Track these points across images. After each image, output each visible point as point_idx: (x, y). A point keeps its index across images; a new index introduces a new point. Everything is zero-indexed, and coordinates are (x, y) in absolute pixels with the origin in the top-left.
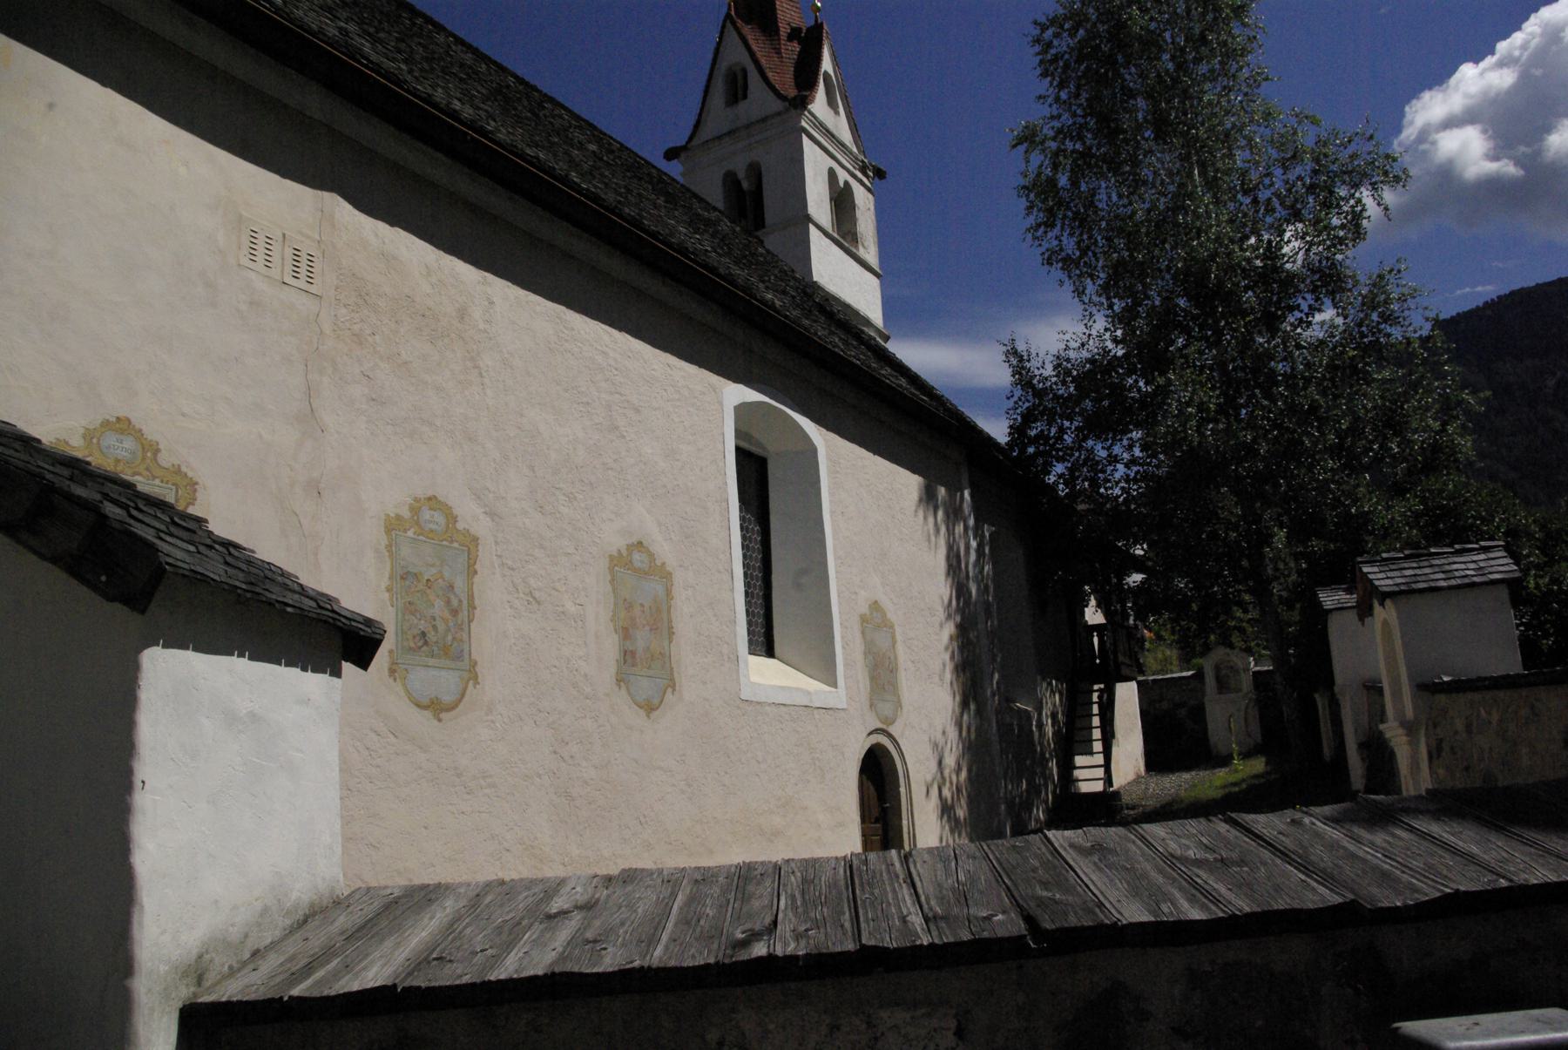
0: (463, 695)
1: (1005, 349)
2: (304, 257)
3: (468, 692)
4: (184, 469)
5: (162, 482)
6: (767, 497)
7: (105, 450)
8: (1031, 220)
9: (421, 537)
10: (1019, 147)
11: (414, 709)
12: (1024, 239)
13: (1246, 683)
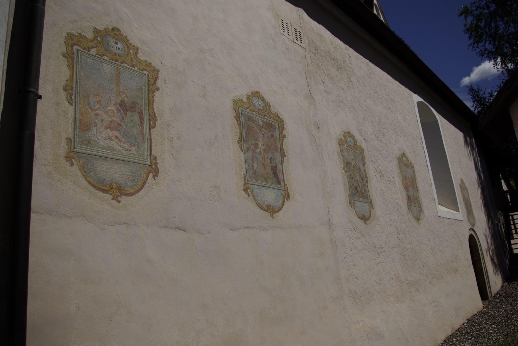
1: (468, 89)
2: (298, 33)
4: (279, 115)
7: (254, 105)
8: (471, 41)
9: (348, 148)
10: (462, 16)
11: (359, 219)
12: (469, 48)
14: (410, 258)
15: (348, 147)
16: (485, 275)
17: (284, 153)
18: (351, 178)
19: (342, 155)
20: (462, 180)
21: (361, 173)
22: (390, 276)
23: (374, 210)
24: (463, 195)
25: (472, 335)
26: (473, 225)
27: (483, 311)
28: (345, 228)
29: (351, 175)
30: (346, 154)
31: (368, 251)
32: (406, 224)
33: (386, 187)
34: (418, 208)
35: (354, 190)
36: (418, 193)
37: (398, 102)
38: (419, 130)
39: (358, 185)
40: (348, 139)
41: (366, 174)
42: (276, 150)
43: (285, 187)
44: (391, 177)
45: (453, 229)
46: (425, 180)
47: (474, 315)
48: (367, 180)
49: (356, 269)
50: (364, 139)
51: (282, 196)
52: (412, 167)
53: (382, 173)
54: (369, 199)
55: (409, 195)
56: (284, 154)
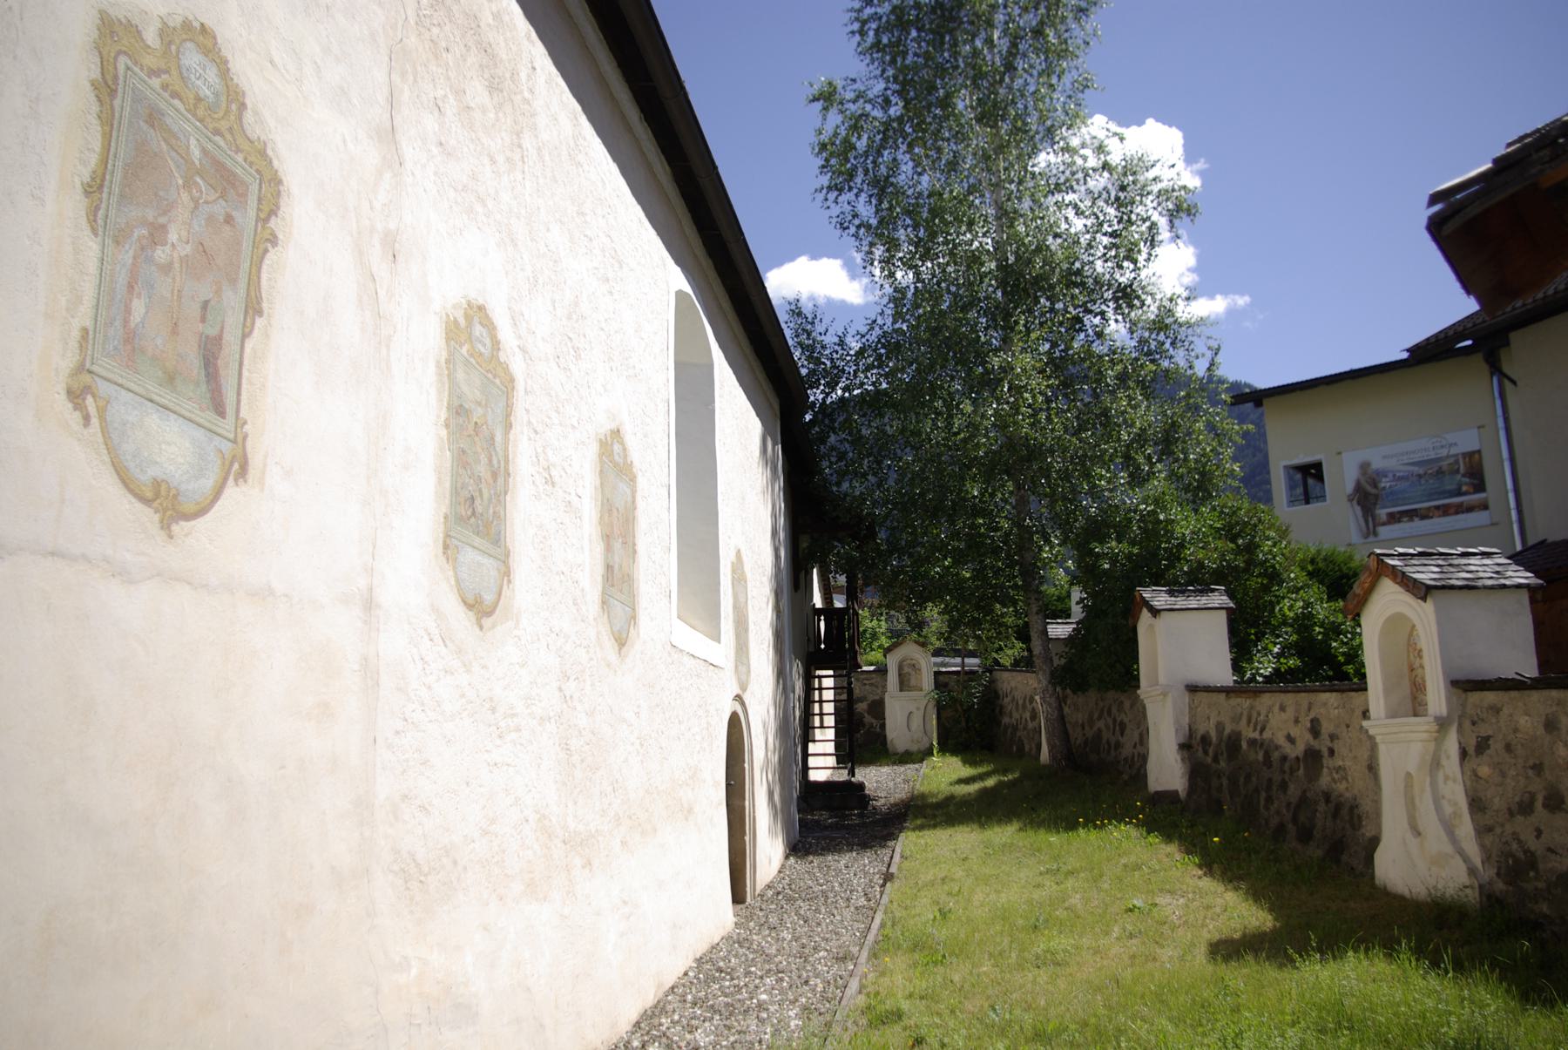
0: (500, 594)
3: (503, 593)
5: (245, 160)
6: (1365, 369)
9: (472, 360)
13: (927, 682)
14: (582, 761)
15: (472, 355)
17: (259, 300)
18: (462, 460)
19: (449, 376)
20: (739, 552)
21: (493, 453)
23: (511, 586)
25: (712, 1006)
26: (744, 687)
27: (735, 938)
30: (460, 375)
31: (472, 720)
33: (555, 520)
34: (627, 609)
39: (480, 491)
40: (478, 330)
42: (233, 281)
43: (239, 430)
44: (573, 493)
48: (506, 483)
50: (523, 349)
51: (219, 462)
52: (633, 479)
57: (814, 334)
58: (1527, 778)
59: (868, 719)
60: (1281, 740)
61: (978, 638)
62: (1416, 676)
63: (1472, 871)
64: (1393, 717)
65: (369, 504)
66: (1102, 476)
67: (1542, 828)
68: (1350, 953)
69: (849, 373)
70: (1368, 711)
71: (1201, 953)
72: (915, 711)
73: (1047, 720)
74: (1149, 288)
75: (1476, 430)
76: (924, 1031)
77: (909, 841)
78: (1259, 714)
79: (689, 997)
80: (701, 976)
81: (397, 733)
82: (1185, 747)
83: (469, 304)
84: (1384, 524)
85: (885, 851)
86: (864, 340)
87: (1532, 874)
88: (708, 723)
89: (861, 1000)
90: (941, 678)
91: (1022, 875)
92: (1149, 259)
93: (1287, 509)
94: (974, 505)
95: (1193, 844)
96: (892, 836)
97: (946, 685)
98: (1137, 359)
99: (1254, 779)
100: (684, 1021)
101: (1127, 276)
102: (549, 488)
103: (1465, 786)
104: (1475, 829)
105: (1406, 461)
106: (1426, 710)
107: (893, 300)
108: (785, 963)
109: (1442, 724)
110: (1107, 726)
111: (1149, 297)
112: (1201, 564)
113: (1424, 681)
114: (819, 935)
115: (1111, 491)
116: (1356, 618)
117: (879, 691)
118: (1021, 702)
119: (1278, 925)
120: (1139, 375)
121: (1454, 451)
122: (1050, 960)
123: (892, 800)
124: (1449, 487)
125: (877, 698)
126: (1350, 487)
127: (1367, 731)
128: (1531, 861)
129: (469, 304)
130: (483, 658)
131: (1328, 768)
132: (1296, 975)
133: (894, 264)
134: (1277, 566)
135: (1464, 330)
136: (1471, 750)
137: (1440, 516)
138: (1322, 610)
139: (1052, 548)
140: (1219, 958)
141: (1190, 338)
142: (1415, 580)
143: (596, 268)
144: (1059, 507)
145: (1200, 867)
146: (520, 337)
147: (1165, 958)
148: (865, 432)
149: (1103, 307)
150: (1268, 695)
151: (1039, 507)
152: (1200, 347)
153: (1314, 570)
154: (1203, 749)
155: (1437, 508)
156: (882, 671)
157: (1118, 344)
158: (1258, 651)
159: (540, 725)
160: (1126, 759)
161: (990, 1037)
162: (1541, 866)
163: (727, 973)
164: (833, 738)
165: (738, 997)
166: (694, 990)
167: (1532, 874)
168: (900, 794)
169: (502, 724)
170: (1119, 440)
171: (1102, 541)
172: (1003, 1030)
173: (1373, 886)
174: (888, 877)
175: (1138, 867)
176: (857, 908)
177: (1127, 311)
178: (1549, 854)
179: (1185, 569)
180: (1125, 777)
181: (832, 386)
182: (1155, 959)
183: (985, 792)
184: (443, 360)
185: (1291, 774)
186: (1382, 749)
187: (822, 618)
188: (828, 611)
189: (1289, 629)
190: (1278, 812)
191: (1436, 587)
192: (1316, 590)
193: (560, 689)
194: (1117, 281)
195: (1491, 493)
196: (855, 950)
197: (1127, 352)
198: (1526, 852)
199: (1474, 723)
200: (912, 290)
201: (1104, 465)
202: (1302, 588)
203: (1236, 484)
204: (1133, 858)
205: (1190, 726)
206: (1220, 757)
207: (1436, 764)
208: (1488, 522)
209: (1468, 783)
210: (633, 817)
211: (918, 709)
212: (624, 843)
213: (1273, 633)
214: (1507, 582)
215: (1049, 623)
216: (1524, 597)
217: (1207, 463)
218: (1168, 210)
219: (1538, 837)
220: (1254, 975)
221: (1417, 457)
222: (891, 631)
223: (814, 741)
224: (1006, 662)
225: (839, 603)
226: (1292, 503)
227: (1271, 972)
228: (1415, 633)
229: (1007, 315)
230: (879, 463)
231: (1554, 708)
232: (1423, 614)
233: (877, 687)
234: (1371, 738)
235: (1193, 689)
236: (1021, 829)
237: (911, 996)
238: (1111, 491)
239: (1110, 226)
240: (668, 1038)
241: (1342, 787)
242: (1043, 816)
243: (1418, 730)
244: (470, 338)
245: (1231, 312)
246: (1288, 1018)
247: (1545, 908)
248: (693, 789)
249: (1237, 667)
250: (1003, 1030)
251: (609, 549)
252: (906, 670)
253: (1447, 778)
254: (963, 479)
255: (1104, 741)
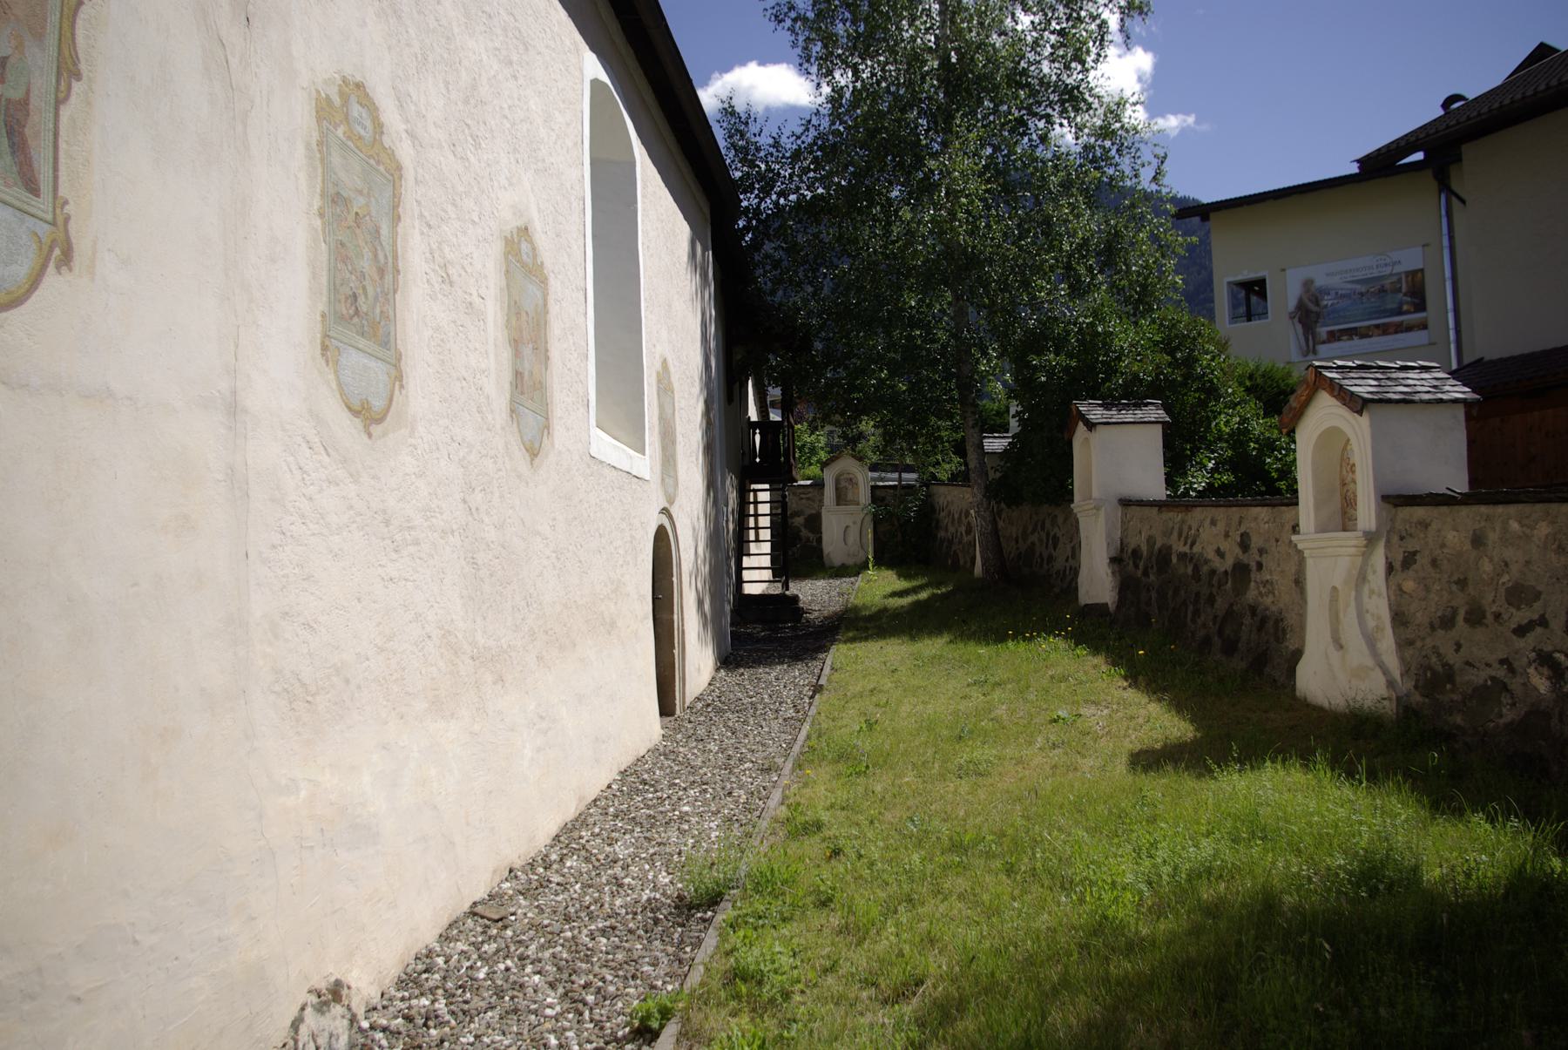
0: (391, 400)
3: (395, 399)
9: (349, 143)
13: (864, 496)
14: (491, 575)
15: (349, 138)
16: (676, 645)
17: (75, 61)
18: (341, 254)
19: (322, 160)
20: (665, 362)
21: (379, 248)
22: (423, 628)
23: (404, 392)
24: (661, 407)
25: (634, 818)
26: (671, 501)
27: (662, 749)
28: (290, 437)
29: (342, 244)
30: (336, 160)
31: (361, 533)
32: (495, 463)
33: (454, 322)
34: (539, 417)
35: (346, 302)
36: (546, 369)
37: (539, 53)
38: (582, 170)
39: (364, 288)
40: (356, 110)
41: (397, 256)
42: (39, 37)
43: (58, 211)
44: (475, 294)
45: (621, 501)
46: (572, 334)
47: (640, 760)
48: (395, 281)
49: (312, 594)
50: (412, 135)
51: (34, 246)
52: (544, 281)
53: (450, 272)
54: (393, 351)
55: (521, 370)
56: (75, 64)
57: (748, 135)
58: (1451, 593)
59: (805, 533)
60: (1210, 554)
61: (915, 452)
62: (1348, 491)
63: (1391, 684)
64: (1324, 531)
65: (229, 299)
66: (1042, 287)
67: (1462, 642)
68: (1268, 763)
69: (785, 177)
70: (1298, 525)
71: (1121, 767)
72: (851, 524)
73: (981, 534)
74: (1097, 90)
75: (1421, 248)
76: (842, 842)
77: (839, 654)
78: (1190, 528)
79: (612, 809)
80: (625, 788)
81: (274, 547)
82: (1114, 560)
83: (344, 80)
84: (1324, 342)
85: (815, 663)
86: (799, 142)
87: (1448, 686)
88: (632, 537)
89: (783, 812)
90: (878, 492)
91: (950, 687)
92: (1098, 60)
93: (1228, 326)
94: (912, 317)
95: (1120, 657)
96: (824, 649)
97: (883, 499)
98: (1081, 166)
99: (1182, 592)
100: (605, 834)
101: (1074, 77)
102: (446, 287)
103: (1389, 600)
104: (1396, 643)
105: (1349, 279)
106: (1356, 524)
107: (831, 100)
108: (709, 775)
109: (1371, 539)
110: (1040, 540)
111: (1096, 101)
112: (1136, 376)
113: (1355, 496)
114: (745, 746)
115: (1051, 302)
116: (1291, 433)
117: (816, 506)
118: (956, 516)
119: (1199, 735)
120: (1083, 182)
121: (1398, 269)
122: (975, 771)
123: (826, 613)
124: (1389, 306)
125: (814, 512)
126: (1292, 304)
127: (1296, 545)
128: (1449, 674)
129: (344, 80)
130: (372, 468)
131: (1255, 581)
132: (1212, 784)
133: (832, 62)
134: (1215, 380)
135: (1417, 140)
136: (1397, 565)
137: (1379, 335)
138: (1258, 426)
139: (989, 361)
140: (1139, 768)
141: (1136, 145)
142: (1352, 393)
143: (497, 49)
144: (999, 319)
145: (1126, 678)
146: (407, 121)
147: (1086, 769)
148: (801, 239)
149: (1049, 111)
150: (1199, 509)
151: (977, 317)
152: (1146, 154)
153: (1252, 386)
154: (1134, 563)
155: (1377, 326)
156: (819, 485)
157: (1062, 150)
158: (1192, 466)
159: (441, 538)
160: (1058, 572)
161: (906, 848)
162: (1458, 679)
163: (652, 786)
164: (769, 551)
165: (661, 809)
166: (616, 803)
167: (1448, 686)
168: (836, 607)
169: (398, 537)
170: (1061, 250)
171: (1039, 353)
172: (920, 841)
173: (1294, 697)
174: (817, 689)
175: (1064, 679)
176: (785, 720)
177: (1072, 115)
178: (1467, 667)
179: (1120, 382)
180: (1057, 590)
181: (766, 192)
182: (1076, 769)
183: (917, 603)
184: (314, 143)
185: (1219, 588)
186: (1310, 563)
187: (758, 431)
188: (764, 424)
189: (1225, 445)
190: (1204, 625)
191: (1372, 401)
192: (1253, 406)
193: (464, 501)
194: (1064, 82)
195: (1431, 314)
196: (779, 761)
197: (1071, 158)
198: (1444, 664)
199: (1402, 538)
200: (851, 89)
201: (1044, 276)
202: (1239, 403)
203: (1177, 297)
204: (1060, 670)
205: (1121, 540)
206: (1150, 571)
207: (1362, 578)
208: (1426, 342)
209: (1393, 598)
210: (550, 632)
211: (854, 523)
212: (540, 658)
213: (1208, 448)
214: (1444, 397)
215: (985, 437)
216: (1460, 412)
217: (1149, 274)
218: (1120, 7)
219: (1457, 651)
220: (1173, 785)
221: (1360, 275)
222: (832, 446)
223: (749, 555)
224: (944, 476)
225: (775, 416)
226: (1234, 318)
227: (1189, 782)
228: (1349, 447)
229: (949, 118)
230: (815, 270)
231: (1483, 524)
232: (1358, 429)
233: (813, 501)
234: (1300, 552)
235: (1126, 503)
236: (951, 641)
237: (832, 806)
238: (1051, 302)
239: (1058, 24)
240: (587, 850)
241: (1268, 600)
242: (973, 628)
243: (1346, 545)
244: (347, 118)
245: (1184, 131)
246: (1204, 829)
247: (1459, 719)
248: (616, 603)
249: (1170, 482)
250: (920, 841)
251: (517, 354)
252: (843, 484)
253: (1372, 592)
254: (900, 289)
255: (1038, 554)
